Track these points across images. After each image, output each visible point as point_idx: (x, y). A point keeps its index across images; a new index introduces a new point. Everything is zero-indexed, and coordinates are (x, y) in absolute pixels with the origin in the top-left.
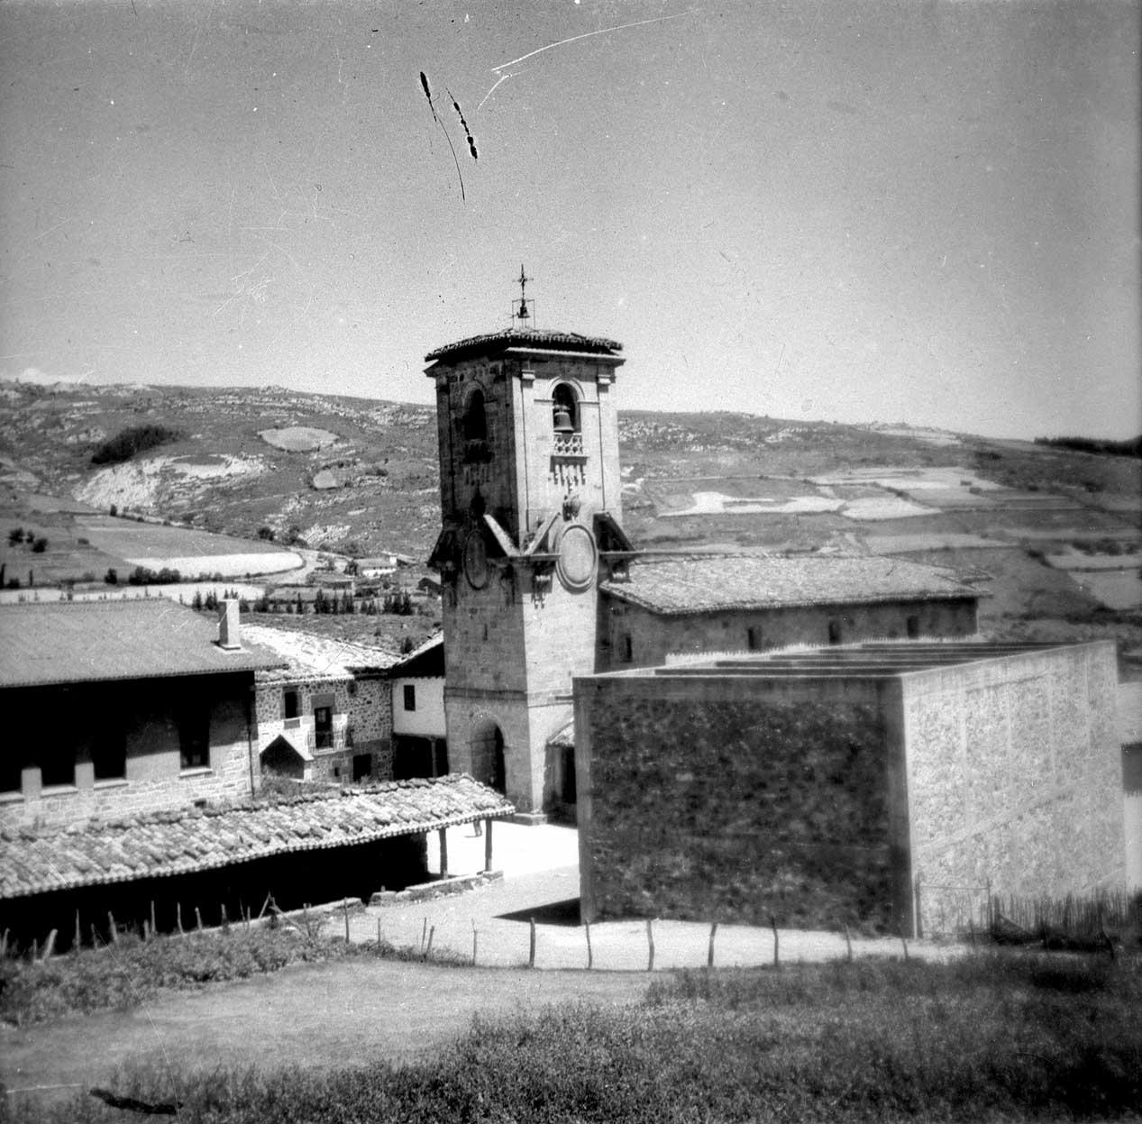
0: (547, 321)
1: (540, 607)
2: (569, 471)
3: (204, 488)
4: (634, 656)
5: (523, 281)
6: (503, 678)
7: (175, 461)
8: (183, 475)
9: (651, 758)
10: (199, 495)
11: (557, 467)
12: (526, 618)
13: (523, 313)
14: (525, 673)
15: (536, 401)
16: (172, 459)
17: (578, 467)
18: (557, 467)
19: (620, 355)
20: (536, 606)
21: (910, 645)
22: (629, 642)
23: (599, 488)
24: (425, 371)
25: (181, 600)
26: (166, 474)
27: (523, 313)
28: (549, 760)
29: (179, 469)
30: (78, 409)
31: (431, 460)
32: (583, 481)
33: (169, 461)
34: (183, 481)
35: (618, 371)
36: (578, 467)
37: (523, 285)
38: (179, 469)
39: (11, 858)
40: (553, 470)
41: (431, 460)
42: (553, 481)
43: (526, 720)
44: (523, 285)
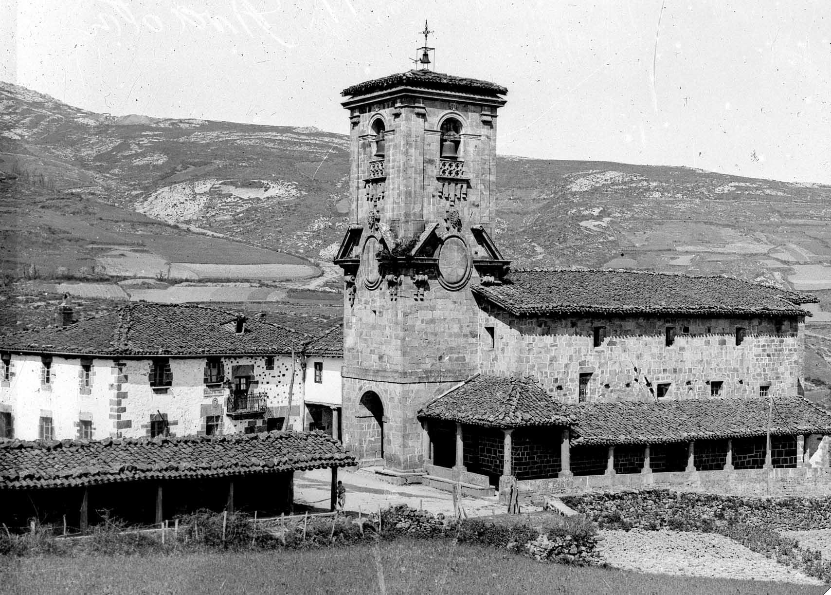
2: (451, 190)
3: (246, 207)
5: (426, 33)
6: (385, 359)
7: (221, 184)
8: (230, 196)
9: (698, 205)
10: (240, 213)
13: (425, 59)
16: (220, 182)
19: (503, 98)
20: (392, 300)
26: (214, 193)
27: (425, 59)
29: (226, 189)
30: (146, 136)
31: (779, 476)
33: (218, 183)
34: (229, 200)
35: (500, 111)
37: (426, 36)
38: (226, 189)
41: (779, 476)
44: (426, 36)
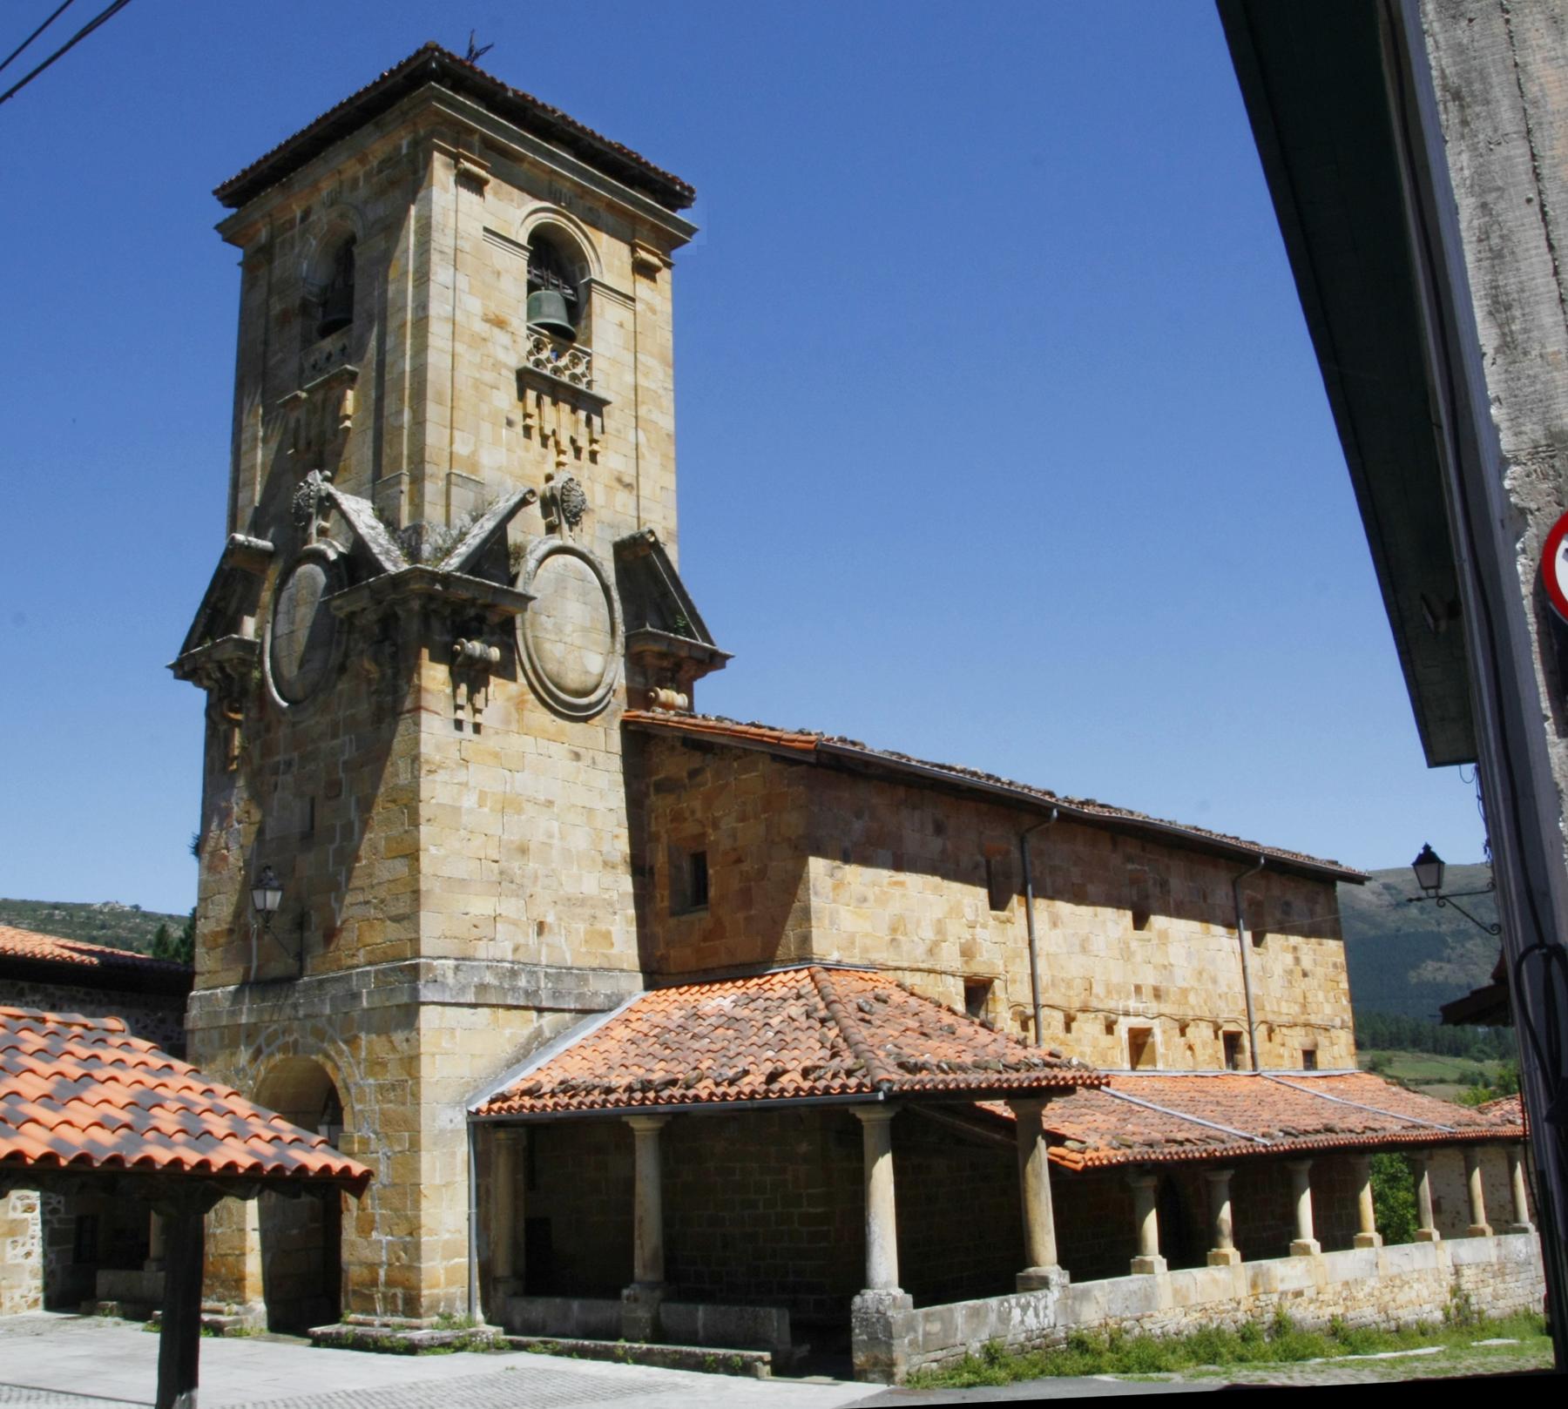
0: (488, 325)
1: (468, 729)
2: (559, 419)
4: (712, 892)
11: (531, 395)
12: (427, 748)
14: (415, 822)
15: (486, 229)
17: (582, 414)
18: (531, 395)
21: (1512, 903)
22: (699, 862)
23: (628, 486)
24: (218, 227)
25: (80, 1099)
28: (482, 1164)
32: (593, 456)
36: (582, 414)
39: (433, 1308)
40: (521, 396)
42: (519, 430)
43: (417, 842)
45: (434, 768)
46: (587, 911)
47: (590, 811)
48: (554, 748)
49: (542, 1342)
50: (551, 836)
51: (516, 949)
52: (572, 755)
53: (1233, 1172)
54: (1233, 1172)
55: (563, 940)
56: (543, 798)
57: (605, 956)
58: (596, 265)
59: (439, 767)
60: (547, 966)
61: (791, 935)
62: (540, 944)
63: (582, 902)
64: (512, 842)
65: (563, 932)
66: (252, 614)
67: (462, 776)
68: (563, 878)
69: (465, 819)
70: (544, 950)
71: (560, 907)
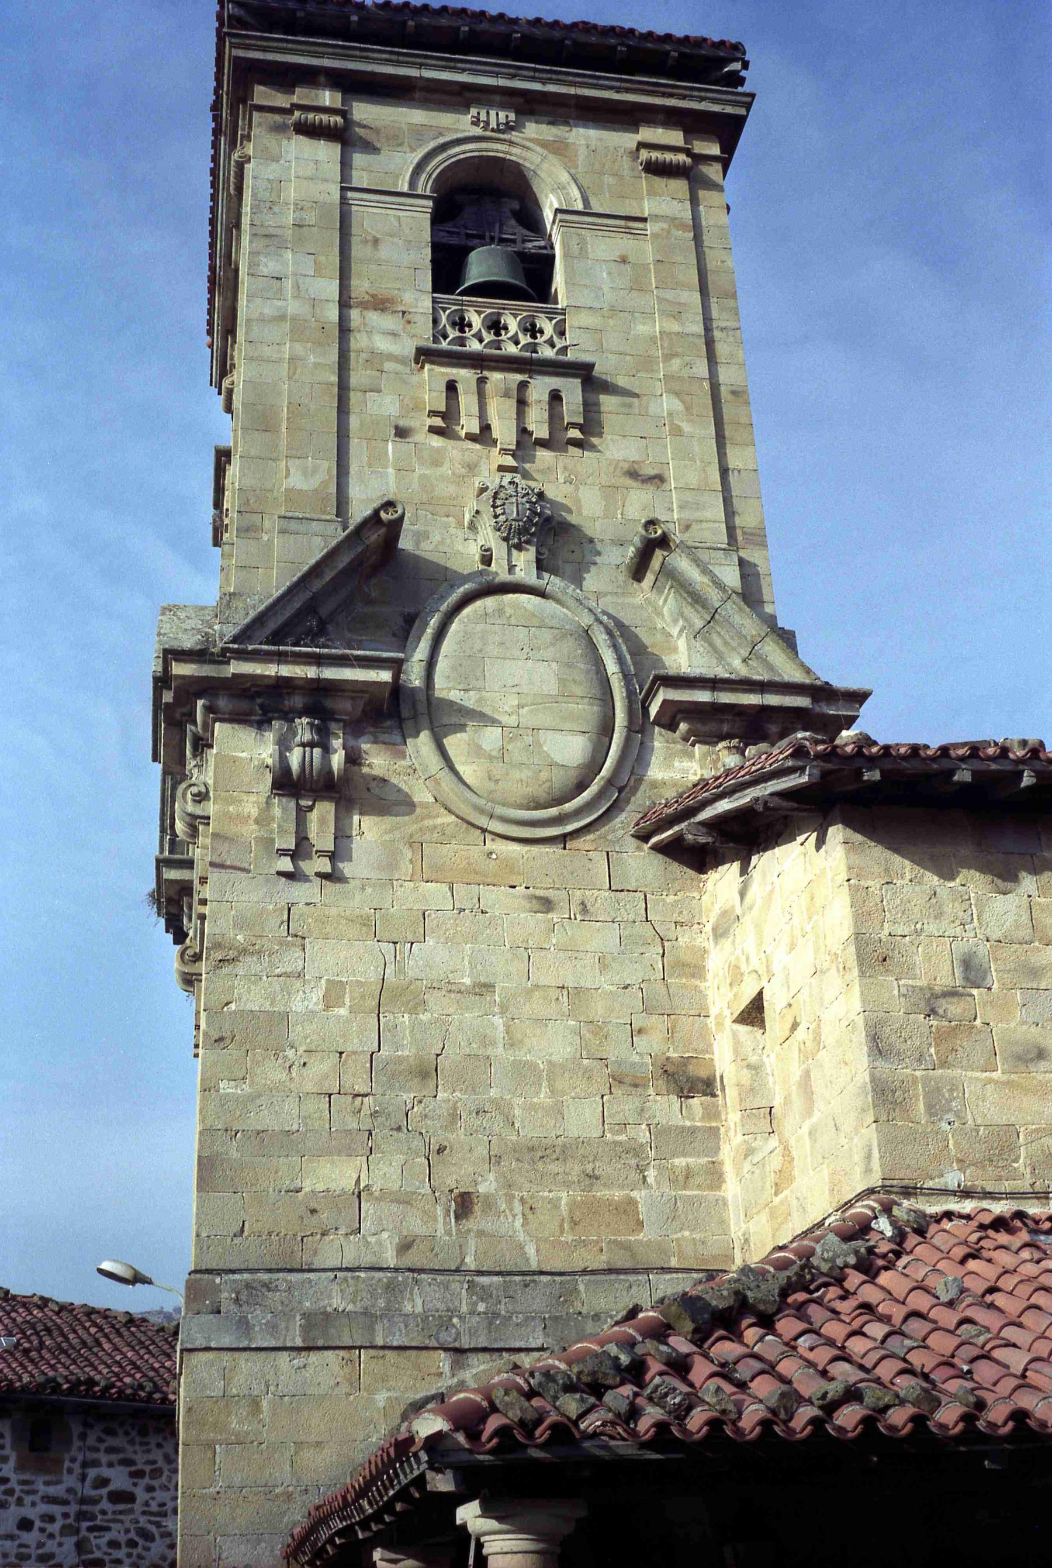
45: (232, 954)
46: (575, 1169)
47: (576, 994)
48: (495, 897)
49: (600, 838)
50: (486, 1041)
51: (405, 1247)
52: (535, 905)
53: (1023, 785)
54: (1023, 785)
55: (518, 1222)
56: (467, 981)
57: (627, 1247)
58: (515, 150)
59: (244, 951)
60: (480, 1273)
61: (751, 741)
62: (463, 1234)
63: (564, 1152)
64: (400, 1060)
65: (518, 1208)
66: (167, 704)
67: (293, 959)
68: (517, 1112)
69: (297, 1032)
70: (472, 1244)
71: (509, 1164)
